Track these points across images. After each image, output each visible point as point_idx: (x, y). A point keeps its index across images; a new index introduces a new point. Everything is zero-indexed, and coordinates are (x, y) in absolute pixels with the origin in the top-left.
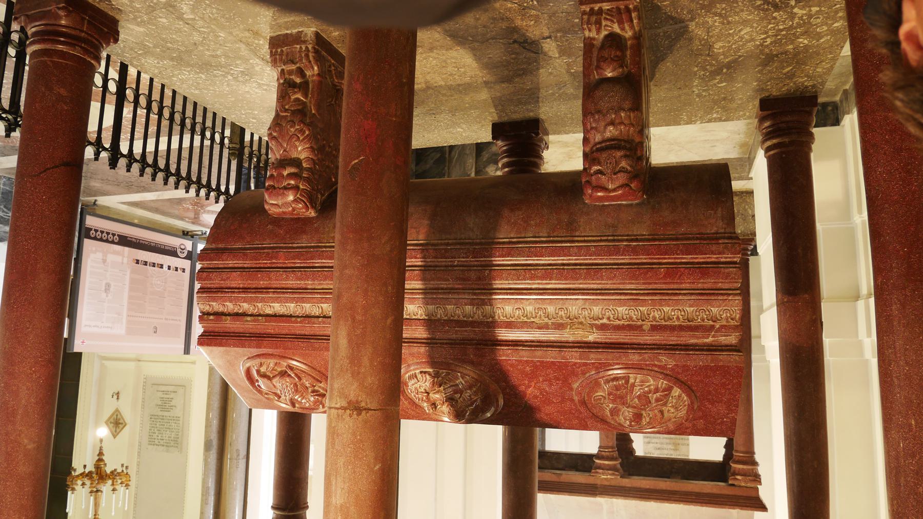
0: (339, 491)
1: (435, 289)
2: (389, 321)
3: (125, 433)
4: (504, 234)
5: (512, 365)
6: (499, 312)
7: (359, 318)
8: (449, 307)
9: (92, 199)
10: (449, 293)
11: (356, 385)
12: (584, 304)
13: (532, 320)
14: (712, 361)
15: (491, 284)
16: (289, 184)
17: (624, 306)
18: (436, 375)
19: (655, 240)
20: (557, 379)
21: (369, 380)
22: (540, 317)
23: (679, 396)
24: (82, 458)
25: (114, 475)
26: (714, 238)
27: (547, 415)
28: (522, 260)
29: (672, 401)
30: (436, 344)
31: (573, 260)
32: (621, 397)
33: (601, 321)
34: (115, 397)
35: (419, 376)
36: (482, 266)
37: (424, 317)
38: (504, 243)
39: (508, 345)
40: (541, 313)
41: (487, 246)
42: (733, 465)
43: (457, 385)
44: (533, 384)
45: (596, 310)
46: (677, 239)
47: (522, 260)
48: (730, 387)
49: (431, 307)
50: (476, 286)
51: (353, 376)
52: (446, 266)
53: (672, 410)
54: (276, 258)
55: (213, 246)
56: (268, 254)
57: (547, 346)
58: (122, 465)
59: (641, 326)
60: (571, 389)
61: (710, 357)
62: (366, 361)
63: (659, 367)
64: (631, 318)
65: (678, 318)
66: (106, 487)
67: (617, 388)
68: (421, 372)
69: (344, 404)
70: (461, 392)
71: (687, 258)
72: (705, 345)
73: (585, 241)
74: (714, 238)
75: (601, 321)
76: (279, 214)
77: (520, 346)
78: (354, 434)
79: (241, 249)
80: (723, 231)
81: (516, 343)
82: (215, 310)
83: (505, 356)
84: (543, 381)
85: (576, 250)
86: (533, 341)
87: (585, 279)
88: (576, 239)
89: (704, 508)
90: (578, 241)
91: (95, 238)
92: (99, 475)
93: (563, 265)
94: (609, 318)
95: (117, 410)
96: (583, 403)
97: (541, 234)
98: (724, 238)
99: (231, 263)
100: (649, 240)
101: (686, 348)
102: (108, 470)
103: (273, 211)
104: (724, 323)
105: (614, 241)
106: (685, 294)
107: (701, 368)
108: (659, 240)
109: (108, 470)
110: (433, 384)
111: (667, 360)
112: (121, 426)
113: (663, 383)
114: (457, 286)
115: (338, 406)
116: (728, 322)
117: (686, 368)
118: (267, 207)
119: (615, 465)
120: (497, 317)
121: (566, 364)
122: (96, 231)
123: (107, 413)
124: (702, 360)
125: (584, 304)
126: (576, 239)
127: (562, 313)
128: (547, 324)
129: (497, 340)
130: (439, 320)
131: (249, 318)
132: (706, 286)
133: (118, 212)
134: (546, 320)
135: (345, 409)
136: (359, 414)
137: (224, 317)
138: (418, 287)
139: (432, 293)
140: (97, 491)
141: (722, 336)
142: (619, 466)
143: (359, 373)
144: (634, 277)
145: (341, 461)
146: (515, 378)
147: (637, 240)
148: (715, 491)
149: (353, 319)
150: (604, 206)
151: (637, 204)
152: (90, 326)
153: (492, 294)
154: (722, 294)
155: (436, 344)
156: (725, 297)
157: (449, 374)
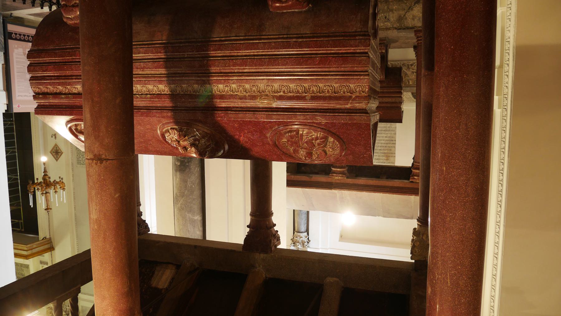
0: (94, 211)
1: (174, 74)
2: (118, 101)
3: (63, 158)
4: (217, 35)
5: (226, 123)
6: (215, 88)
7: (96, 99)
8: (184, 86)
9: (9, 12)
10: (183, 76)
11: (97, 144)
12: (268, 82)
13: (236, 93)
14: (350, 120)
15: (209, 70)
16: (75, 3)
17: (294, 83)
18: (180, 131)
19: (313, 37)
20: (256, 131)
21: (106, 141)
22: (241, 91)
23: (334, 142)
24: (38, 175)
25: (55, 183)
26: (353, 35)
27: (257, 153)
28: (227, 53)
29: (329, 145)
30: (178, 110)
31: (260, 52)
32: (296, 143)
33: (279, 94)
34: (54, 137)
35: (170, 131)
36: (202, 57)
37: (169, 93)
38: (216, 41)
39: (222, 111)
40: (241, 89)
41: (205, 43)
42: (413, 171)
43: (195, 136)
44: (242, 134)
45: (276, 86)
46: (329, 36)
47: (227, 53)
48: (364, 136)
49: (173, 86)
50: (200, 72)
51: (95, 138)
52: (180, 58)
53: (331, 150)
54: (75, 56)
55: (36, 48)
56: (69, 52)
57: (246, 111)
58: (60, 177)
59: (305, 96)
60: (267, 138)
61: (348, 117)
62: (103, 128)
63: (317, 123)
64: (298, 92)
65: (328, 91)
66: (52, 191)
67: (292, 137)
68: (171, 128)
69: (92, 156)
70: (199, 140)
71: (335, 50)
72: (346, 109)
73: (268, 39)
74: (353, 35)
75: (279, 94)
76: (73, 24)
77: (230, 110)
78: (99, 175)
79: (52, 49)
80: (359, 30)
81: (227, 109)
82: (43, 91)
83: (221, 118)
84: (248, 133)
85: (262, 45)
86: (237, 108)
87: (268, 65)
88: (263, 37)
89: (395, 195)
90: (264, 39)
91: (16, 39)
92: (47, 184)
93: (254, 55)
94: (284, 92)
95: (56, 145)
96: (275, 145)
97: (240, 34)
98: (360, 35)
99: (47, 59)
100: (309, 37)
101: (334, 111)
102: (52, 180)
103: (70, 22)
104: (358, 94)
105: (287, 38)
106: (332, 75)
107: (343, 124)
108: (317, 37)
109: (52, 180)
110: (180, 136)
111: (321, 120)
112: (60, 154)
113: (320, 134)
114: (188, 72)
115: (88, 158)
116: (360, 94)
117: (333, 125)
118: (65, 20)
119: (343, 171)
120: (214, 92)
121: (259, 122)
122: (16, 34)
123: (50, 148)
124: (343, 119)
125: (268, 82)
126: (263, 37)
127: (254, 89)
128: (245, 96)
129: (216, 107)
130: (178, 94)
131: (63, 96)
132: (346, 69)
133: (29, 21)
134: (245, 93)
135: (92, 159)
136: (101, 163)
137: (48, 96)
138: (163, 72)
139: (173, 77)
140: (46, 193)
141: (357, 103)
142: (346, 172)
143: (99, 136)
144: (299, 64)
145: (93, 192)
146: (231, 131)
147: (302, 38)
148: (401, 185)
149: (93, 101)
150: (283, 13)
151: (305, 11)
152: (22, 96)
153: (209, 77)
154: (357, 75)
155: (178, 110)
156: (358, 77)
157: (188, 129)
